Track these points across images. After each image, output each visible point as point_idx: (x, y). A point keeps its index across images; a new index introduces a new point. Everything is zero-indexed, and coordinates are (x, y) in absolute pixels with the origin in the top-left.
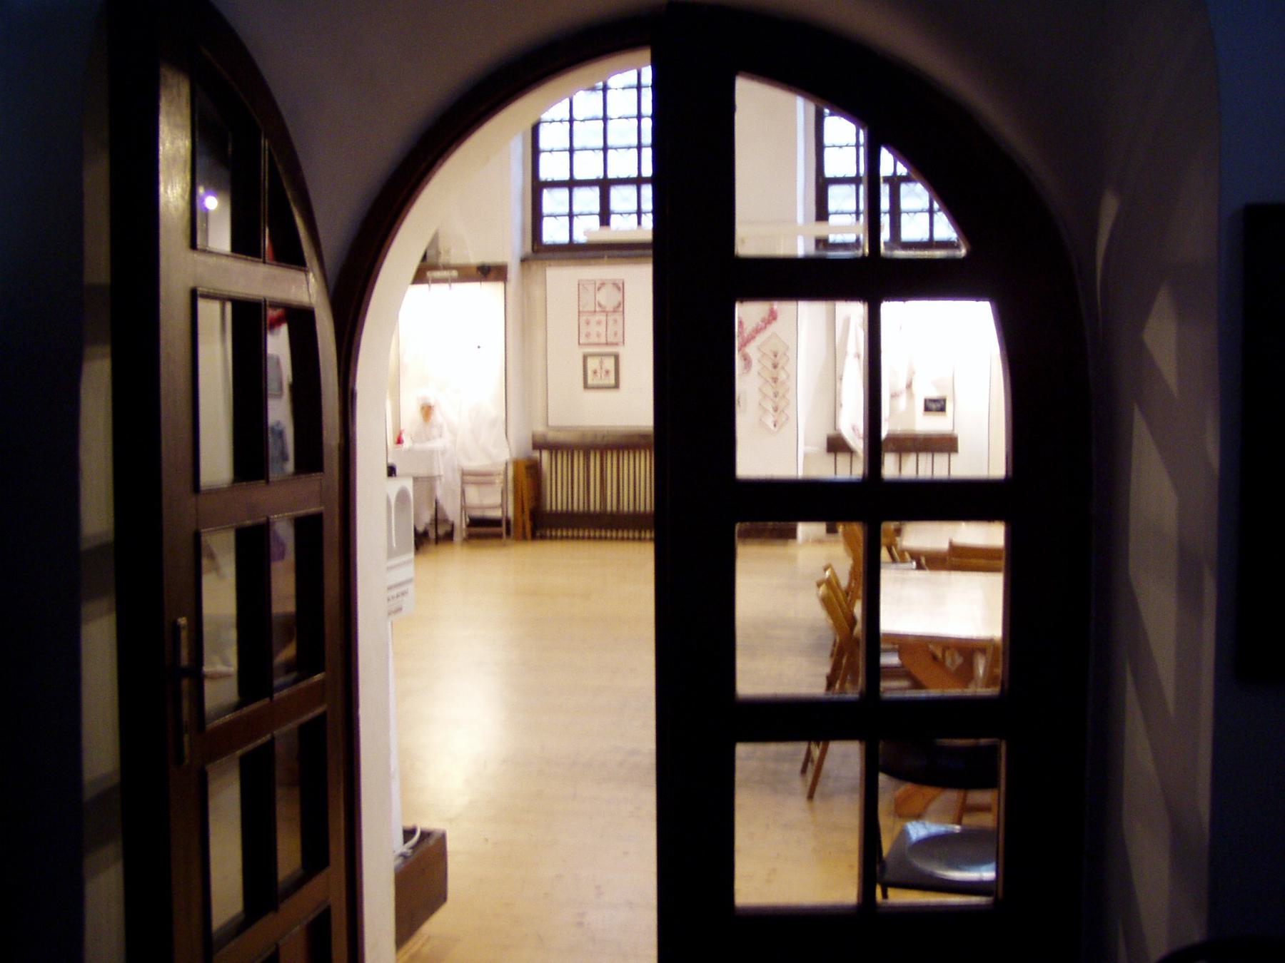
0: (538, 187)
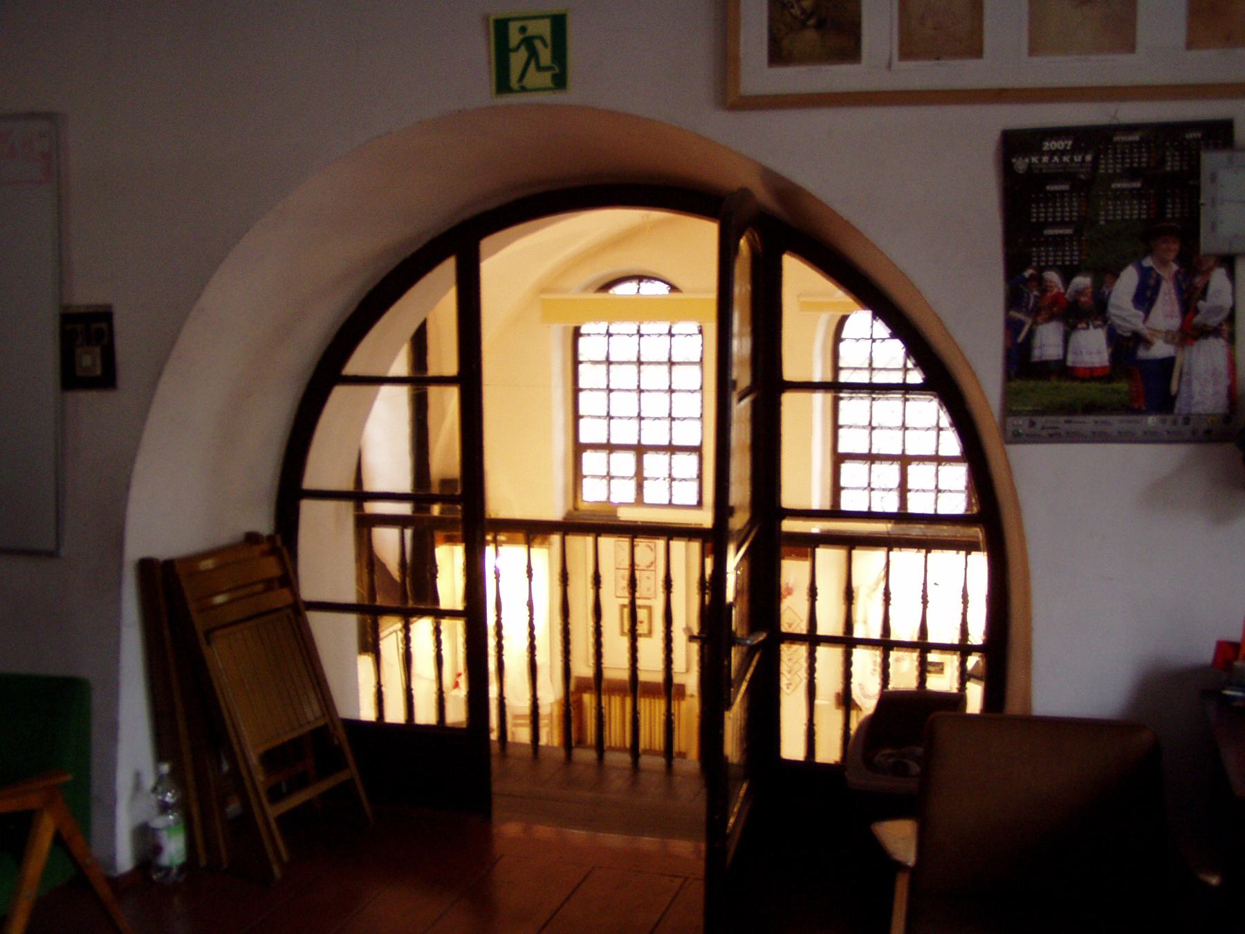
0: (579, 449)
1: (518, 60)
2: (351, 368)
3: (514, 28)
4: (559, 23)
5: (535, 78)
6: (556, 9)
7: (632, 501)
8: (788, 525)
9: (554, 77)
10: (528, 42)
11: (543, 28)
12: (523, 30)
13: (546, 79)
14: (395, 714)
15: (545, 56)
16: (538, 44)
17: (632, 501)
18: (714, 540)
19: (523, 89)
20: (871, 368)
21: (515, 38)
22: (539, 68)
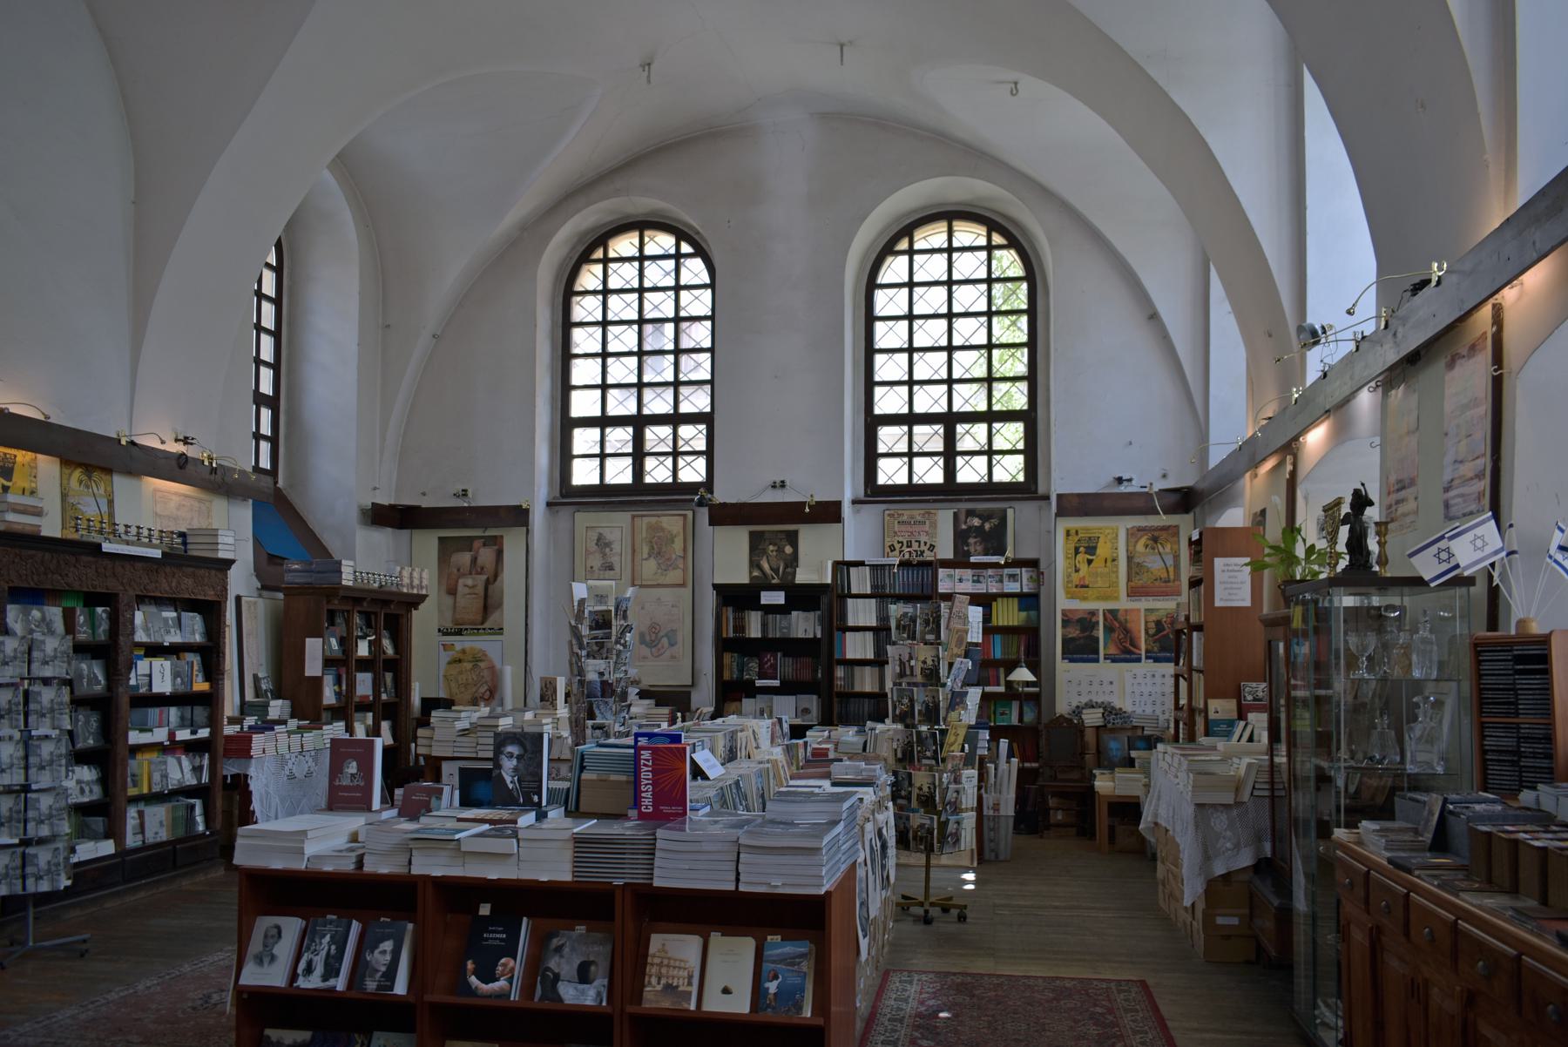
0: (873, 423)
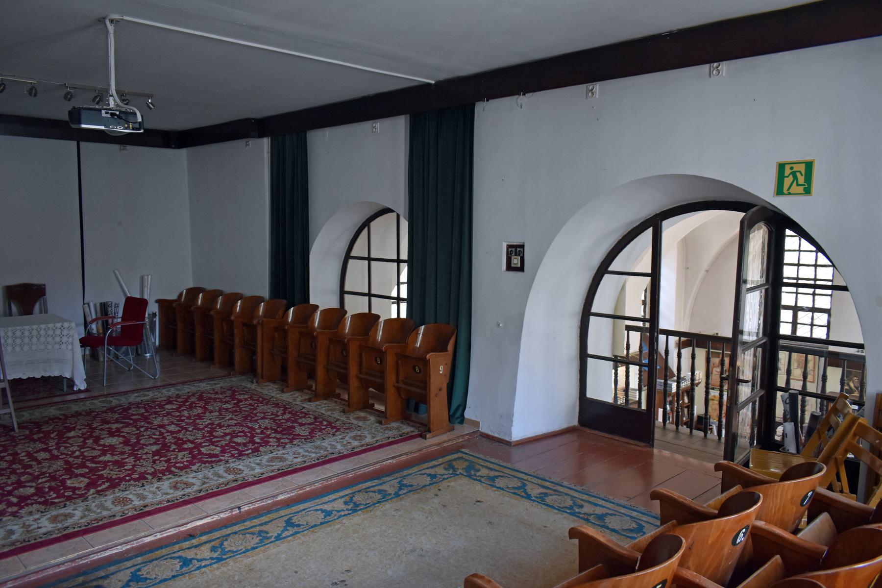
1: (787, 181)
2: (610, 269)
3: (787, 168)
4: (809, 165)
5: (795, 189)
6: (808, 159)
7: (590, 394)
8: (785, 281)
9: (805, 189)
10: (794, 174)
11: (802, 168)
12: (792, 168)
13: (801, 189)
14: (621, 401)
15: (801, 180)
16: (798, 174)
17: (590, 394)
18: (815, 279)
19: (790, 194)
20: (797, 293)
21: (787, 171)
22: (798, 185)
